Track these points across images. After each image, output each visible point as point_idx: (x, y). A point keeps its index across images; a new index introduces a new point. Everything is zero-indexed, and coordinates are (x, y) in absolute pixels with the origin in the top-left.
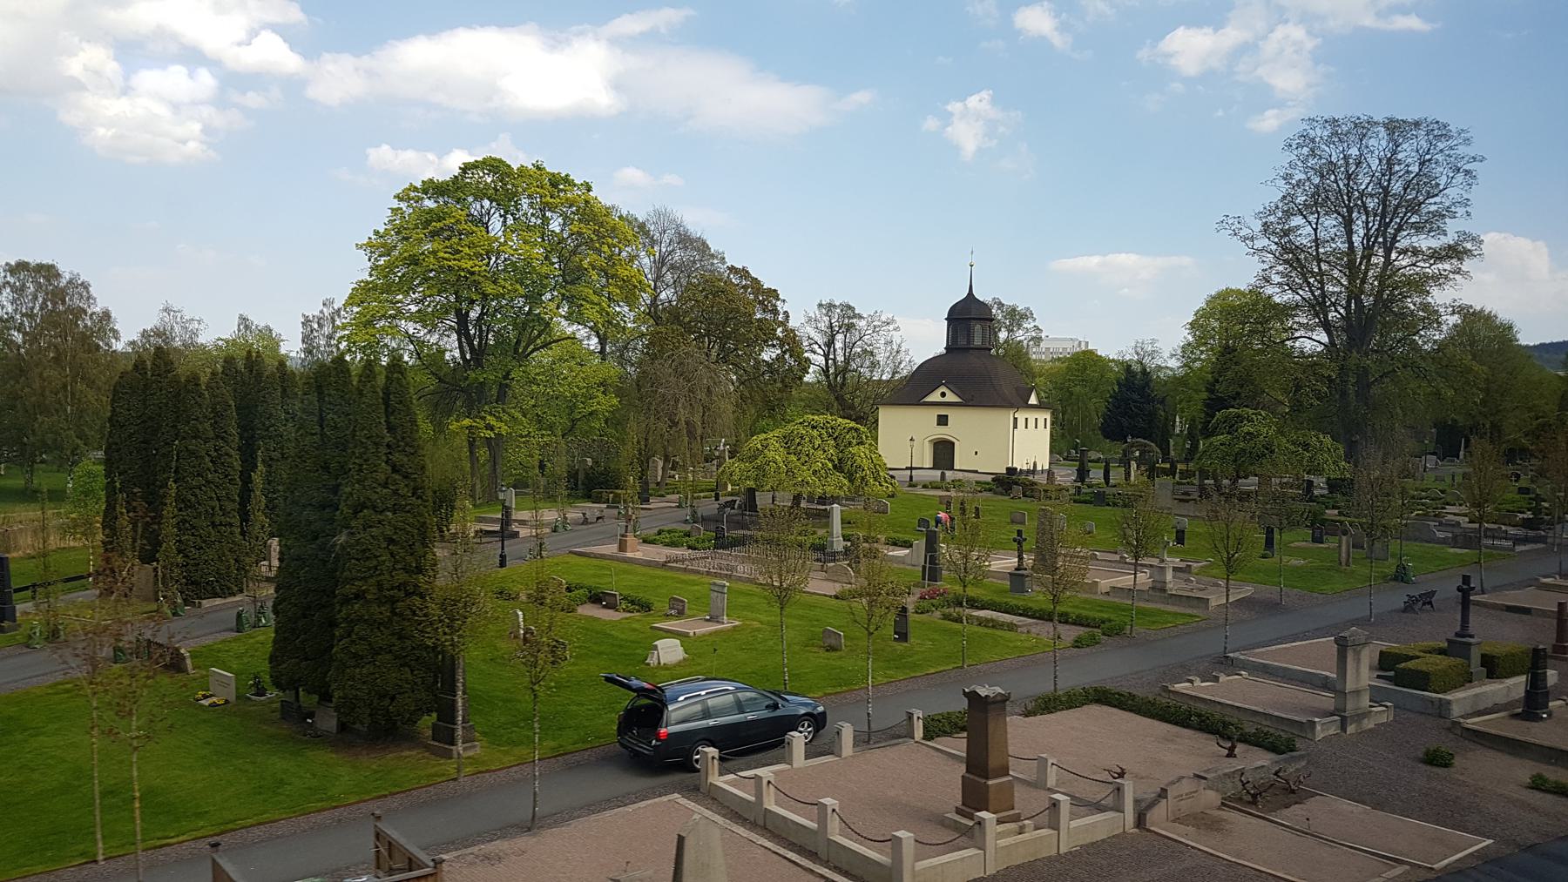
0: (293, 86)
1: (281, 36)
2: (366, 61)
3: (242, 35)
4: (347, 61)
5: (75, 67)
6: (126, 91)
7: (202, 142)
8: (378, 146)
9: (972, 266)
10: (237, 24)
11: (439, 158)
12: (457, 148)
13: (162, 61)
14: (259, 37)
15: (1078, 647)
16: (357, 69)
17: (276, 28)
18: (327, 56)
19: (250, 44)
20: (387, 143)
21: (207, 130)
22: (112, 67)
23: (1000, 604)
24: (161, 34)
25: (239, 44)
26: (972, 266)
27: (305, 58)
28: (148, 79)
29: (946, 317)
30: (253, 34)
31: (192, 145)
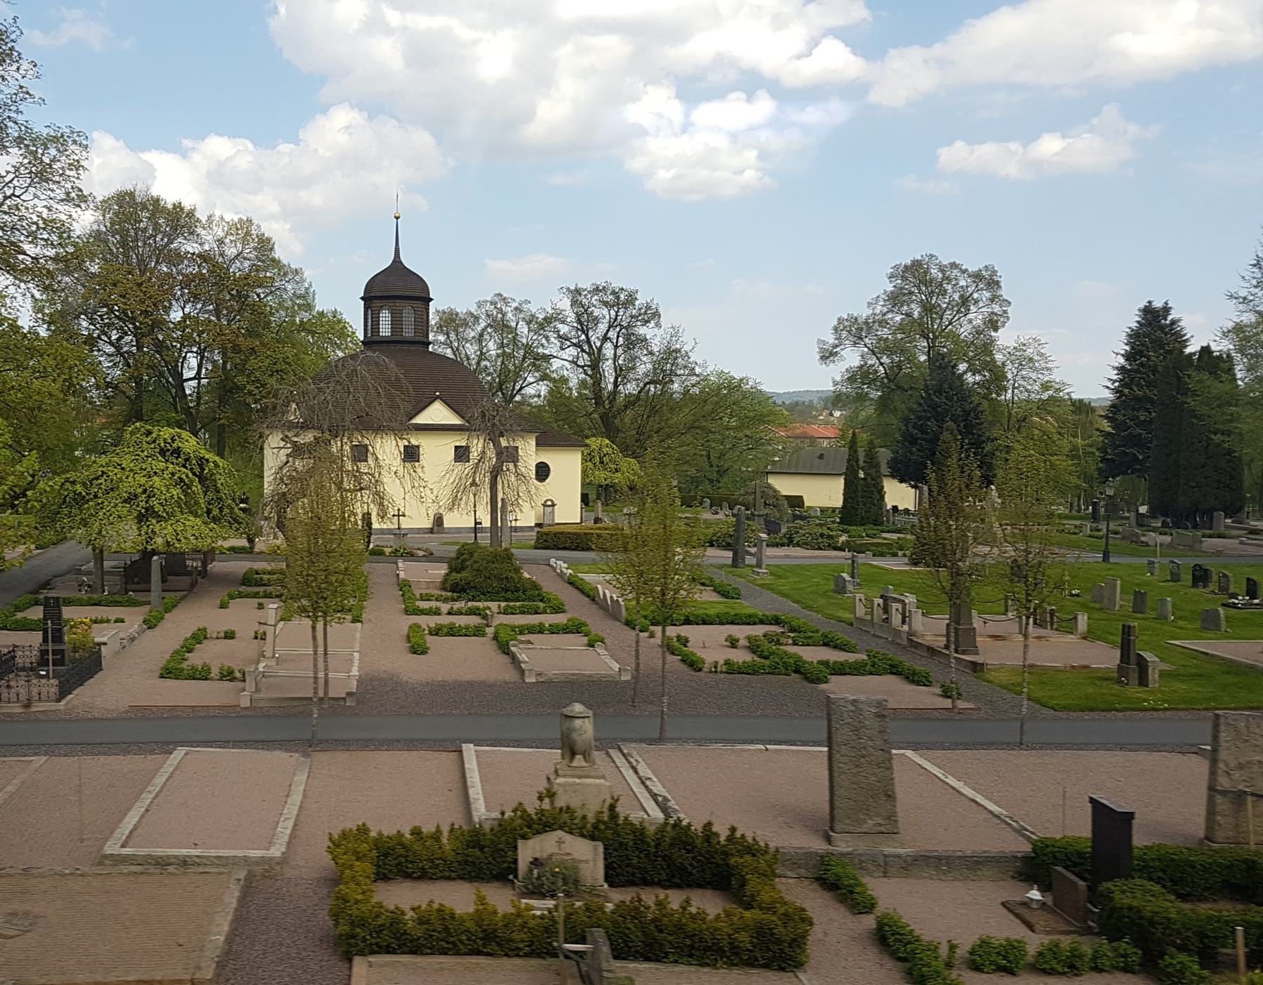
0: (852, 90)
1: (843, 41)
2: (937, 49)
3: (801, 46)
4: (915, 53)
5: (636, 113)
6: (686, 128)
7: (758, 170)
8: (950, 143)
9: (397, 218)
10: (796, 36)
11: (1025, 146)
12: (1047, 132)
13: (719, 93)
14: (820, 47)
15: (1123, 630)
16: (926, 61)
17: (838, 33)
18: (893, 52)
19: (810, 55)
20: (962, 140)
21: (763, 155)
22: (675, 110)
23: (533, 626)
24: (721, 62)
25: (799, 57)
26: (397, 218)
27: (867, 59)
28: (706, 113)
29: (362, 295)
30: (814, 43)
31: (749, 175)
